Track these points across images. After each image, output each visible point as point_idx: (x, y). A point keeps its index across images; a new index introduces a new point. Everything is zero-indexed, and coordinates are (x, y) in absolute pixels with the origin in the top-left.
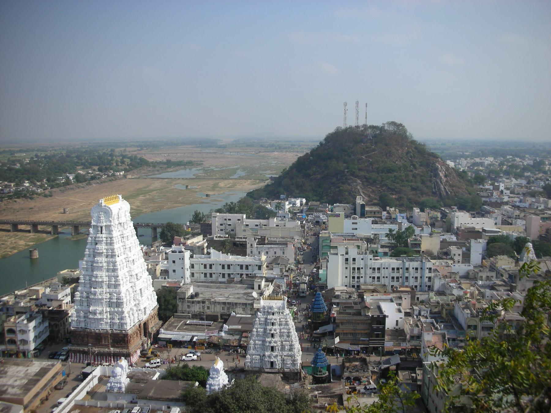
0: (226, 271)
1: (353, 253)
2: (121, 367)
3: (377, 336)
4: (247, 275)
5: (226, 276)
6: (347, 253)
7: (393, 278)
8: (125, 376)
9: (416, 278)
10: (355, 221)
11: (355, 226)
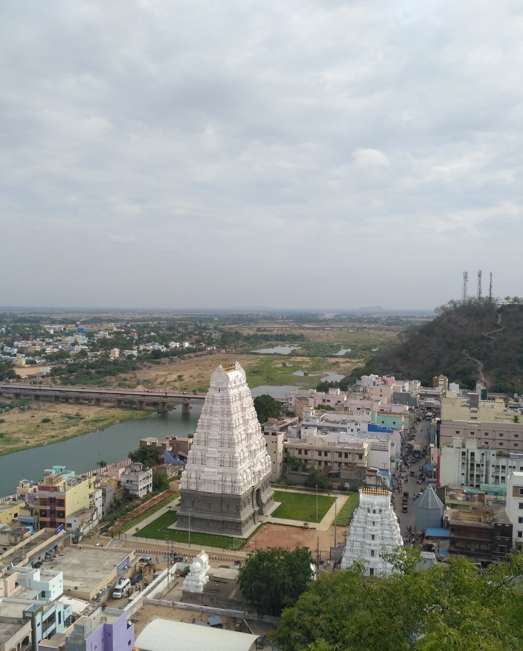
0: (323, 458)
1: (472, 446)
2: (201, 561)
4: (346, 464)
5: (323, 464)
6: (464, 447)
8: (204, 573)
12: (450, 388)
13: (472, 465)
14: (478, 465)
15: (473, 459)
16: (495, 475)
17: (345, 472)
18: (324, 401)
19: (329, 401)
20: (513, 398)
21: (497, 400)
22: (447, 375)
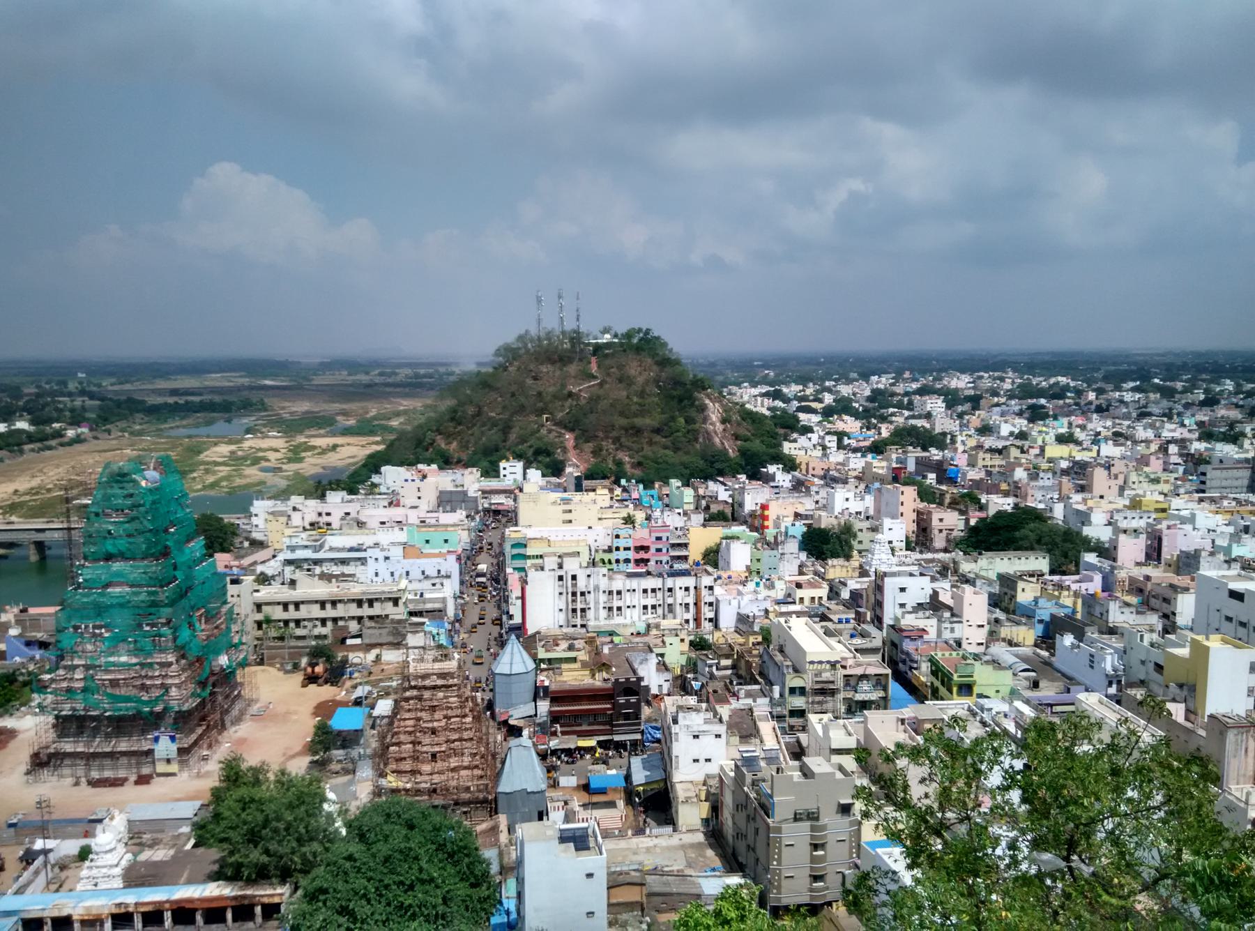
3: (627, 716)
4: (371, 618)
6: (561, 566)
7: (645, 607)
9: (687, 605)
10: (565, 495)
11: (568, 516)
12: (528, 476)
13: (574, 594)
14: (583, 594)
15: (575, 585)
16: (608, 605)
17: (370, 631)
18: (320, 514)
19: (328, 514)
20: (619, 486)
21: (599, 492)
22: (519, 457)
